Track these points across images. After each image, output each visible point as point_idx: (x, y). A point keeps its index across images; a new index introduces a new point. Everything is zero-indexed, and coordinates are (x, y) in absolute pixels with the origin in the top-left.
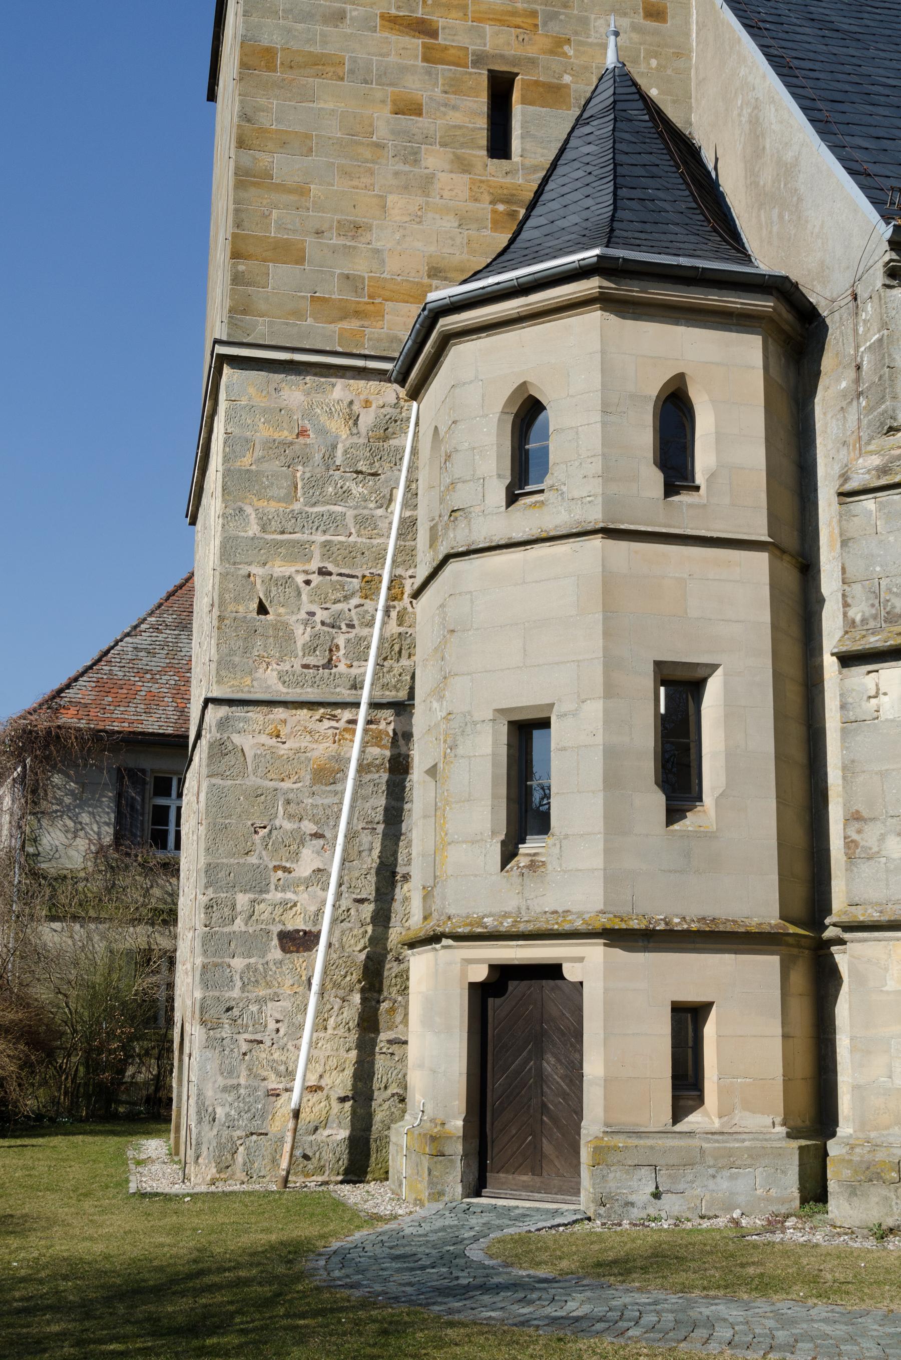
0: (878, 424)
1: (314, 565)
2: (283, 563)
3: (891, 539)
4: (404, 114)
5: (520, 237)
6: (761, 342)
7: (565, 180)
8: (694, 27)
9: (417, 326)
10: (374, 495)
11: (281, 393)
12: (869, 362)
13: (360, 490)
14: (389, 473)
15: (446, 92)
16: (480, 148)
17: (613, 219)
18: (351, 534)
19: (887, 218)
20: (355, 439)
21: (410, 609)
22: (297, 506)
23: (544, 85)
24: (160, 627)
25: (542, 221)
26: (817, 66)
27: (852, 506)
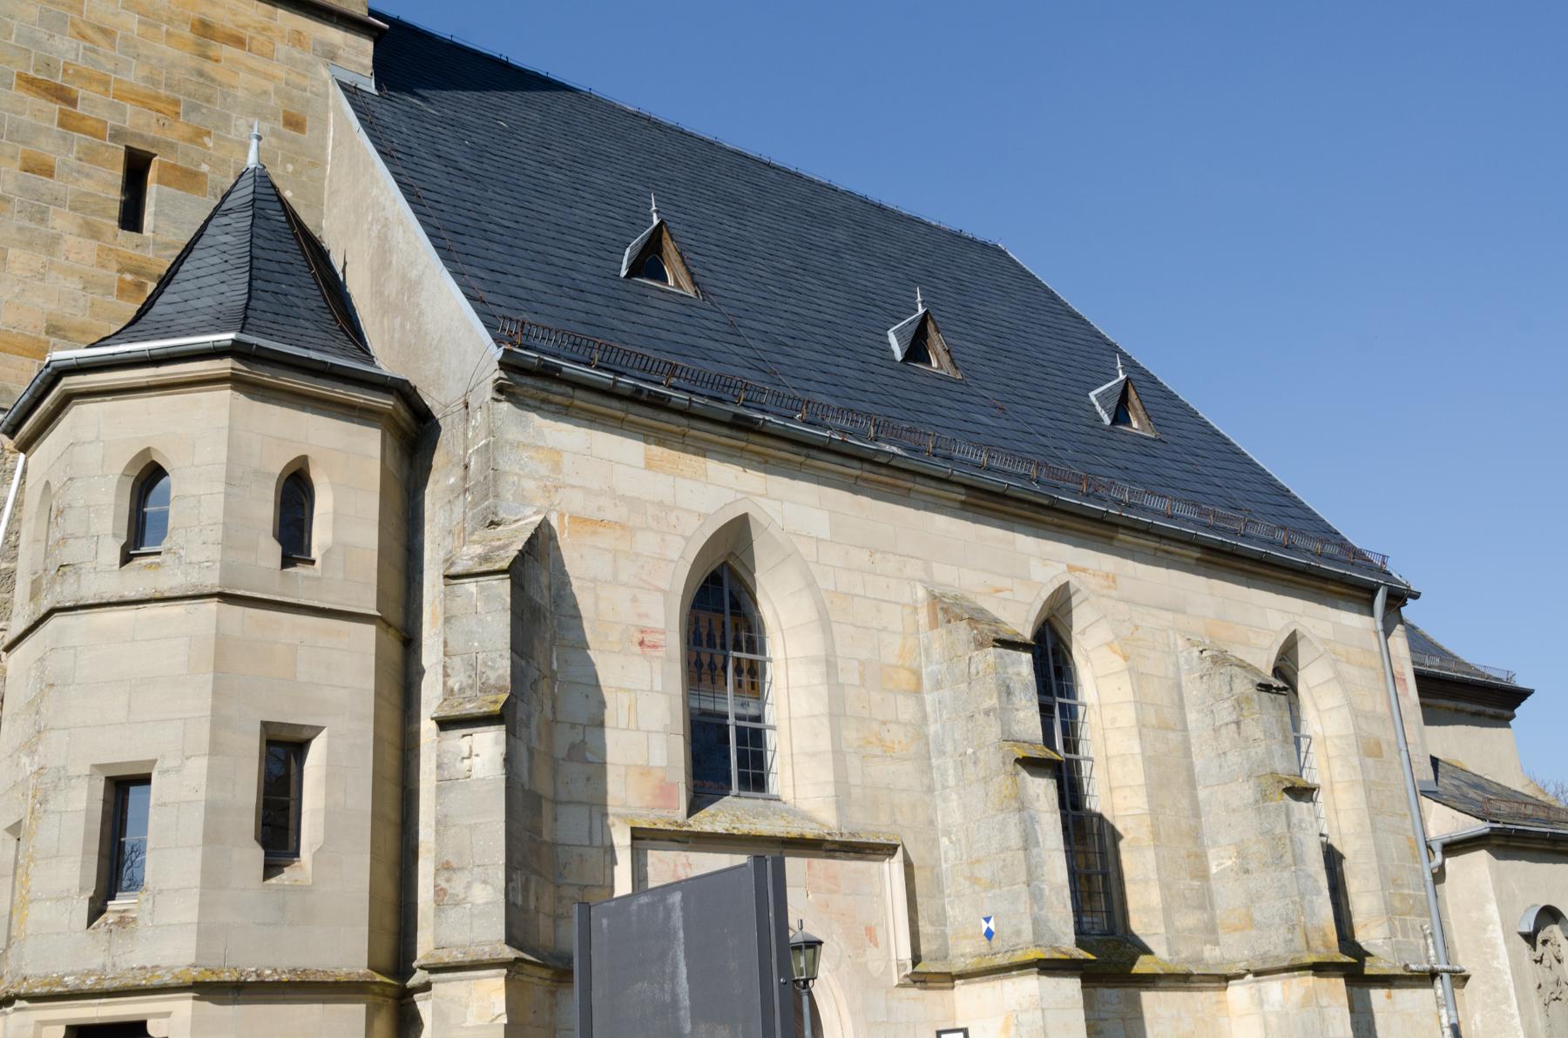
7: (199, 264)
17: (247, 307)
19: (498, 342)
23: (181, 169)
25: (176, 298)
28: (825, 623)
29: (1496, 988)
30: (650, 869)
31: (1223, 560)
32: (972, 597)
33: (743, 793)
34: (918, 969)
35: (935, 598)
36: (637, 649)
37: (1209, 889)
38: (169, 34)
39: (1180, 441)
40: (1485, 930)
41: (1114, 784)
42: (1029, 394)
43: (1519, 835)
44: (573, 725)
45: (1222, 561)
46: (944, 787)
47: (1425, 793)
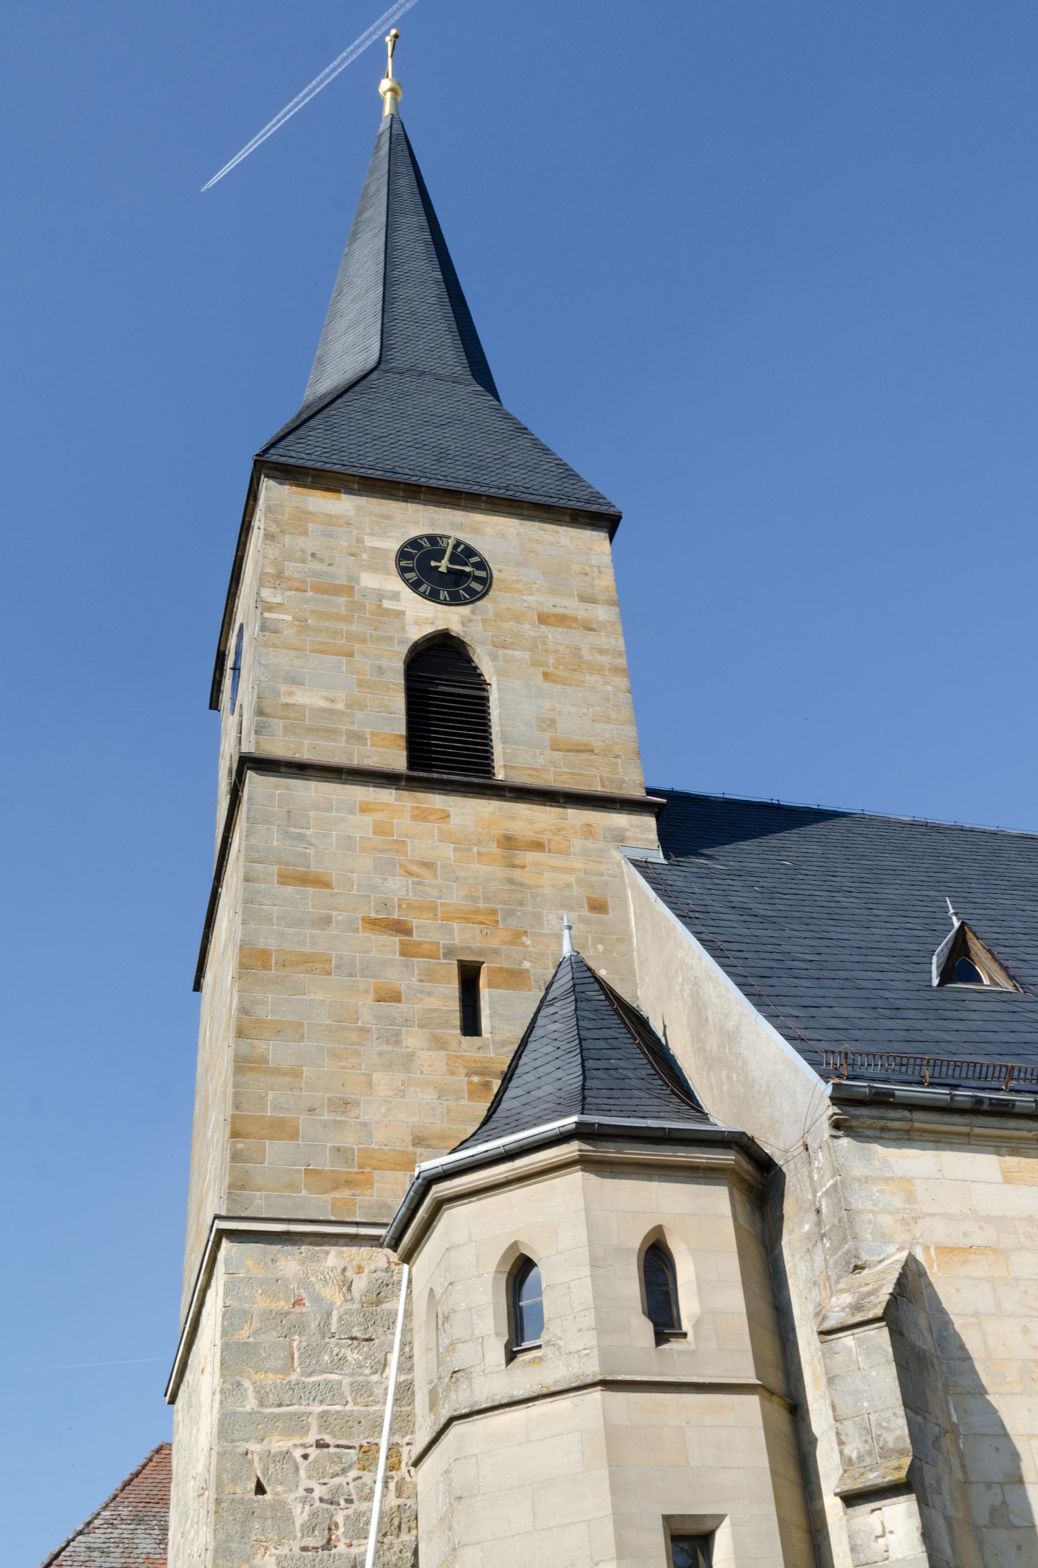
0: (844, 1263)
1: (312, 1438)
2: (281, 1438)
3: (874, 1373)
4: (385, 1001)
5: (501, 1107)
6: (727, 1192)
8: (632, 916)
9: (411, 1193)
10: (369, 1361)
11: (278, 1264)
12: (827, 1206)
13: (355, 1356)
14: (383, 1338)
15: (422, 981)
16: (454, 1027)
17: (583, 1088)
18: (347, 1402)
19: (825, 1077)
20: (349, 1306)
21: (408, 1479)
22: (294, 1377)
23: (507, 970)
24: (115, 1522)
25: (519, 1092)
26: (743, 947)
27: (833, 1344)
38: (480, 854)
44: (989, 1485)
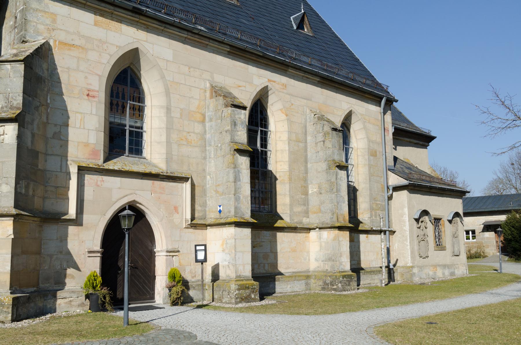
3: (15, 80)
28: (168, 93)
29: (403, 236)
30: (86, 182)
31: (327, 82)
32: (228, 88)
33: (130, 155)
34: (193, 222)
35: (212, 87)
36: (86, 97)
37: (308, 199)
39: (322, 38)
40: (402, 217)
41: (278, 160)
42: (267, 15)
43: (420, 185)
44: (56, 125)
45: (327, 82)
46: (210, 158)
47: (389, 170)
